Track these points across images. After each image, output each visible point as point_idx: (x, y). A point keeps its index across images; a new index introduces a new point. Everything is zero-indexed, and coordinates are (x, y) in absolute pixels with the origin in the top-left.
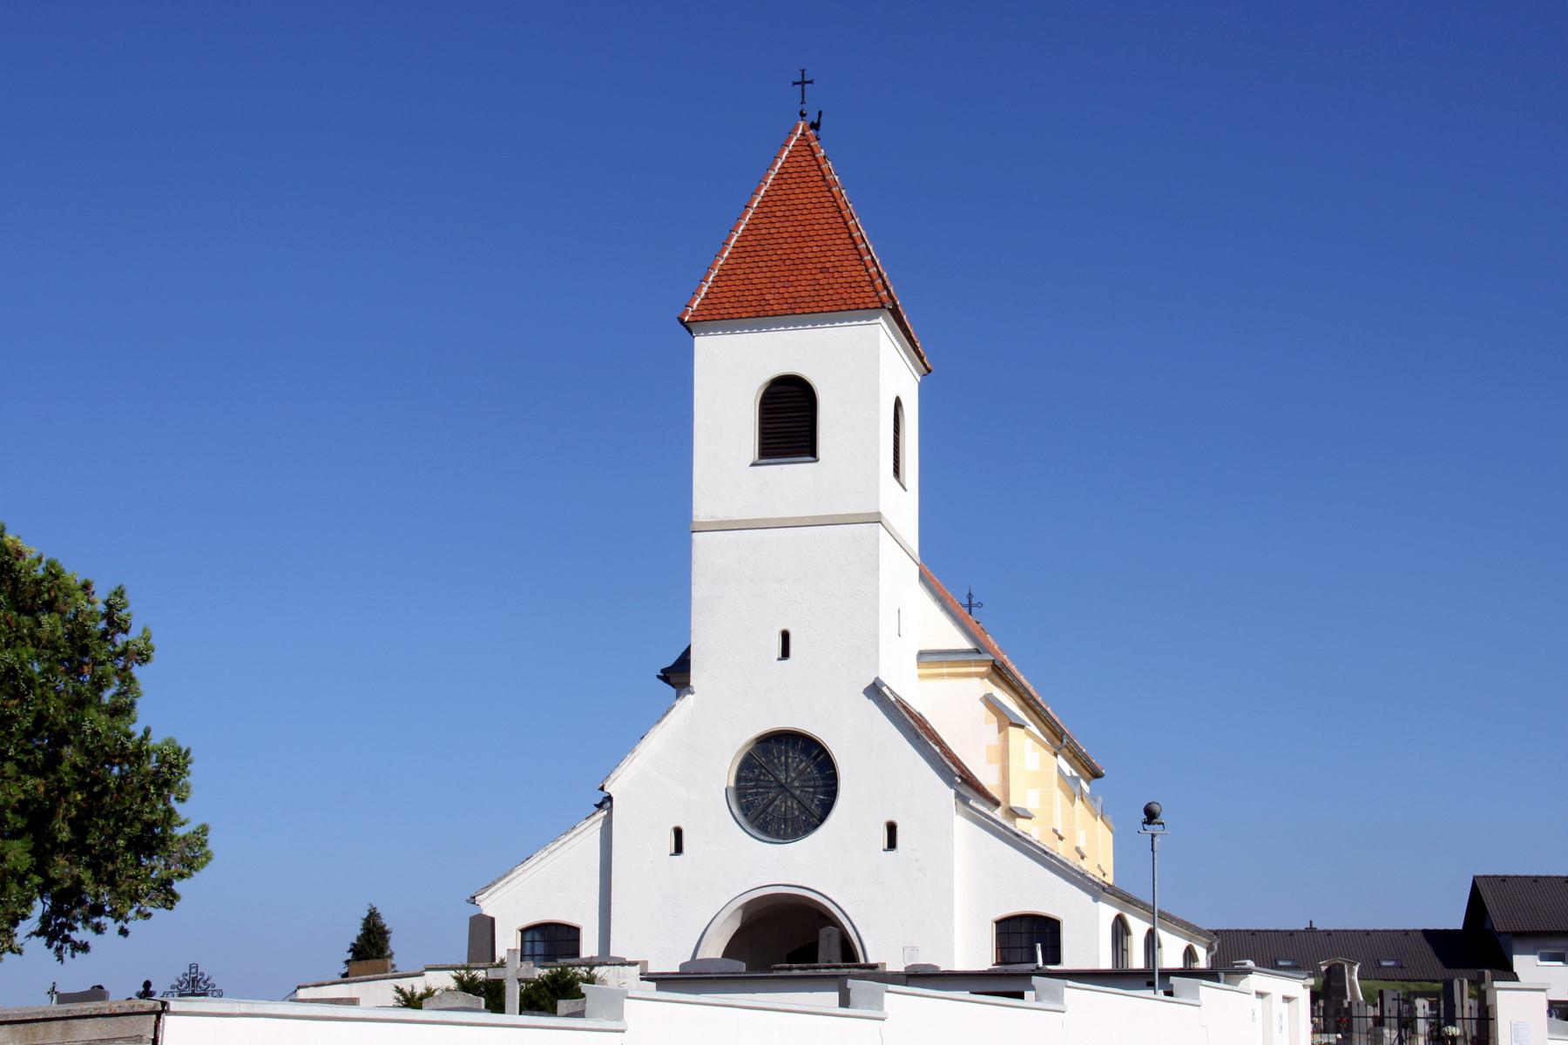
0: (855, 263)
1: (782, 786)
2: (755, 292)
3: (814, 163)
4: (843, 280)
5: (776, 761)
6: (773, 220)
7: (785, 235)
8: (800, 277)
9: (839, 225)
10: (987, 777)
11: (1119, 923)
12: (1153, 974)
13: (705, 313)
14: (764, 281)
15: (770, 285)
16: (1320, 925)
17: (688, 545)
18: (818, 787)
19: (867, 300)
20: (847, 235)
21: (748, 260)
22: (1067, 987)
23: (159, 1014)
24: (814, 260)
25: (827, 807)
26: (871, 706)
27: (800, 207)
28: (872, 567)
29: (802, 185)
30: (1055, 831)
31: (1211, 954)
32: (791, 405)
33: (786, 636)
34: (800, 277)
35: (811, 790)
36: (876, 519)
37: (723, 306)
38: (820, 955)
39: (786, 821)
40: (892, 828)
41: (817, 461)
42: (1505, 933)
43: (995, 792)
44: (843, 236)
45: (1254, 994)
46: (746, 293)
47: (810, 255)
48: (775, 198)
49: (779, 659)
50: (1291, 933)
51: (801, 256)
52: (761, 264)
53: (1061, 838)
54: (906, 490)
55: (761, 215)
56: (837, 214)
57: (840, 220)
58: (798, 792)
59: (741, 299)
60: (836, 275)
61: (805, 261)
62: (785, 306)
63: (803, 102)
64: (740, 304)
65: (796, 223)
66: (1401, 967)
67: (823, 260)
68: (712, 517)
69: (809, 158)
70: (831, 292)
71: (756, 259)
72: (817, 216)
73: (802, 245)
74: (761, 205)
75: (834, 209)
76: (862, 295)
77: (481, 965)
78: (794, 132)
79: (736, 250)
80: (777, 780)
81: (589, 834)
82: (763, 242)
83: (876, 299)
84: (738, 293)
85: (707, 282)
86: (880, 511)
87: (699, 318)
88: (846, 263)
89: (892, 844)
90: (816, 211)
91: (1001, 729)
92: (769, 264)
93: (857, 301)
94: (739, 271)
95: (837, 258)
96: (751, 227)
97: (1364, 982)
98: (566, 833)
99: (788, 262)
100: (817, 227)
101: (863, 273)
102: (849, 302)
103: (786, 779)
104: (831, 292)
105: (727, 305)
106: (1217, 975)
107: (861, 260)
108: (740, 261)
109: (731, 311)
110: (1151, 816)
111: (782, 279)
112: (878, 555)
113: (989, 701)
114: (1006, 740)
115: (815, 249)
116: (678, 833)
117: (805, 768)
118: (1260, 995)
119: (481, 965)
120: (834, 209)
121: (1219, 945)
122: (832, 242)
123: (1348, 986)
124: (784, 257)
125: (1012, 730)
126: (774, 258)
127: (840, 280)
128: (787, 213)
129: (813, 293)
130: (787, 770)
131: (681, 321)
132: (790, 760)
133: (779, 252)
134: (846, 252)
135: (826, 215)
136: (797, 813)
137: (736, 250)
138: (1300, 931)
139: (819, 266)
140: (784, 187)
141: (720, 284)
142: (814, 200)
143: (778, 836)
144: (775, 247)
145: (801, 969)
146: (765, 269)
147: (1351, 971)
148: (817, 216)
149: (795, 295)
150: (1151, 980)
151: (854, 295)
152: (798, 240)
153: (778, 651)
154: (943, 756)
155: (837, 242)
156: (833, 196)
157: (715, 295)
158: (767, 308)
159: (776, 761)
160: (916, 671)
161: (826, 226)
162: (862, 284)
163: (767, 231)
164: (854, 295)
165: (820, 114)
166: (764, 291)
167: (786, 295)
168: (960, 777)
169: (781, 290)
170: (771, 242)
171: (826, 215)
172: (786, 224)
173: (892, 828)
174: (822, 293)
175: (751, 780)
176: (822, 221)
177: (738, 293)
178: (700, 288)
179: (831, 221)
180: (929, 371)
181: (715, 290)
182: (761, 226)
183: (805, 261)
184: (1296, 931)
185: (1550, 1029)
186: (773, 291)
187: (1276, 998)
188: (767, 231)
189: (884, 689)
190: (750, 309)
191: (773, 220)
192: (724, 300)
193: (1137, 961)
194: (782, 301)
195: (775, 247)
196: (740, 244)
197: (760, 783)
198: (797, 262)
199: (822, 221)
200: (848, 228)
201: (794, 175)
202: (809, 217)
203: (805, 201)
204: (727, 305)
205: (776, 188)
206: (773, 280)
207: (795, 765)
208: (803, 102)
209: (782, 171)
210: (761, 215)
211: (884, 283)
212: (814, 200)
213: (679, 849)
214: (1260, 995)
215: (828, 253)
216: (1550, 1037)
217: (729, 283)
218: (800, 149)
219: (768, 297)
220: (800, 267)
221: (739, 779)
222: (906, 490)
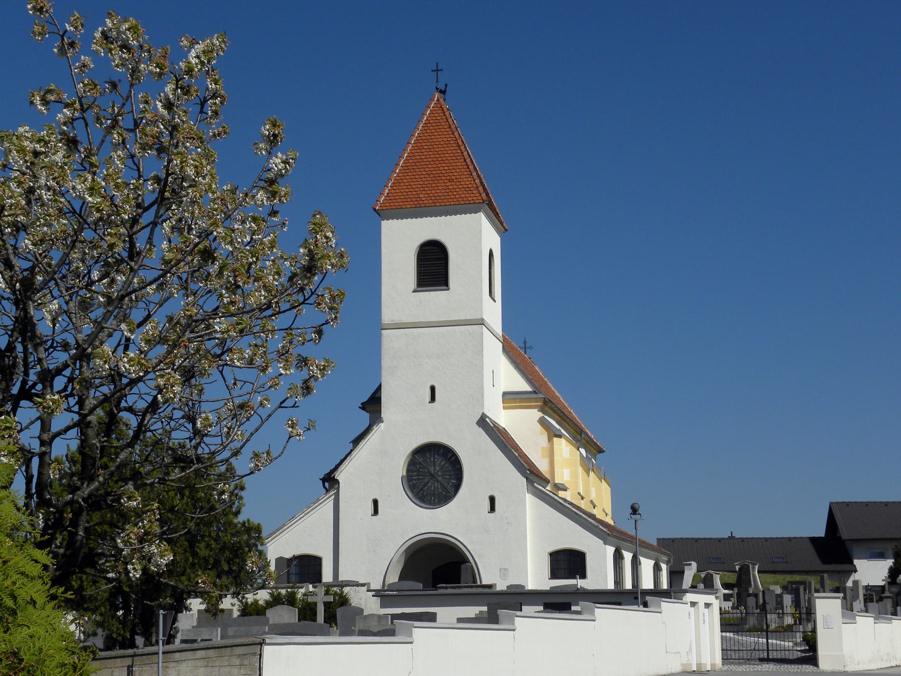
0: (468, 176)
1: (432, 475)
2: (414, 193)
3: (444, 117)
4: (462, 186)
5: (428, 460)
6: (423, 151)
7: (430, 160)
8: (438, 185)
9: (458, 154)
10: (542, 466)
11: (617, 554)
12: (638, 593)
13: (387, 205)
14: (419, 186)
15: (422, 189)
16: (737, 535)
17: (380, 337)
18: (452, 475)
19: (474, 198)
20: (463, 160)
21: (409, 174)
22: (596, 607)
23: (261, 644)
24: (446, 175)
25: (457, 487)
26: (480, 430)
27: (437, 143)
28: (479, 350)
29: (438, 130)
30: (579, 494)
31: (669, 565)
32: (433, 257)
33: (433, 389)
34: (438, 185)
35: (448, 477)
36: (481, 322)
37: (396, 201)
38: (462, 579)
39: (434, 495)
40: (492, 500)
41: (448, 289)
42: (848, 540)
43: (547, 475)
44: (461, 161)
45: (689, 604)
46: (409, 193)
47: (443, 172)
48: (423, 138)
49: (429, 402)
50: (720, 540)
51: (438, 172)
52: (417, 177)
53: (582, 498)
54: (495, 301)
55: (416, 148)
56: (457, 148)
57: (459, 151)
58: (440, 479)
59: (407, 197)
60: (458, 183)
61: (441, 175)
62: (430, 202)
63: (437, 82)
64: (406, 200)
65: (435, 153)
66: (787, 562)
67: (450, 174)
68: (392, 321)
69: (441, 114)
70: (455, 193)
71: (414, 174)
72: (447, 149)
73: (439, 165)
74: (417, 142)
75: (456, 145)
76: (472, 195)
77: (282, 585)
78: (432, 100)
79: (403, 168)
80: (429, 472)
81: (329, 505)
82: (417, 164)
83: (480, 198)
84: (404, 194)
85: (388, 187)
86: (484, 318)
87: (384, 208)
88: (462, 177)
89: (492, 509)
90: (446, 146)
91: (550, 440)
92: (421, 176)
93: (469, 199)
94: (405, 181)
95: (458, 174)
96: (411, 155)
97: (761, 575)
98: (314, 503)
99: (431, 176)
100: (446, 155)
101: (472, 182)
102: (465, 199)
103: (434, 471)
104: (455, 193)
105: (399, 200)
106: (671, 594)
107: (471, 175)
108: (406, 174)
109: (401, 204)
110: (634, 511)
111: (429, 185)
112: (482, 343)
113: (542, 422)
114: (552, 444)
115: (446, 168)
116: (375, 502)
117: (445, 465)
118: (693, 604)
119: (282, 585)
120: (456, 145)
121: (674, 559)
122: (455, 164)
123: (752, 578)
124: (429, 173)
125: (555, 440)
126: (424, 173)
127: (460, 187)
128: (430, 147)
129: (445, 194)
130: (434, 465)
131: (375, 210)
132: (436, 460)
133: (426, 170)
134: (462, 170)
135: (451, 148)
136: (440, 490)
137: (403, 168)
138: (725, 539)
139: (448, 178)
140: (428, 131)
141: (395, 188)
142: (445, 139)
143: (430, 504)
144: (424, 166)
145: (453, 588)
146: (419, 180)
147: (754, 569)
148: (447, 149)
149: (436, 195)
150: (636, 596)
151: (467, 196)
152: (437, 162)
153: (428, 398)
154: (520, 458)
155: (458, 164)
156: (455, 137)
157: (392, 195)
158: (421, 202)
159: (428, 460)
160: (502, 405)
161: (451, 155)
162: (472, 189)
163: (419, 157)
164: (467, 196)
165: (446, 85)
166: (419, 192)
167: (431, 195)
168: (529, 470)
169: (428, 192)
170: (422, 163)
171: (451, 148)
172: (430, 153)
173: (492, 500)
174: (450, 194)
175: (415, 472)
176: (449, 152)
177: (404, 194)
178: (384, 190)
179: (454, 152)
180: (506, 230)
181: (393, 191)
182: (416, 154)
183: (441, 175)
184: (723, 539)
185: (843, 616)
186: (424, 192)
187: (701, 605)
188: (419, 157)
189: (487, 419)
190: (411, 203)
191: (423, 151)
192: (397, 197)
193: (628, 585)
194: (428, 199)
195: (424, 166)
196: (405, 165)
197: (420, 473)
198: (437, 175)
199: (449, 152)
200: (463, 156)
201: (434, 125)
202: (442, 149)
203: (440, 140)
204: (399, 200)
205: (424, 132)
206: (424, 186)
207: (437, 464)
208: (437, 82)
209: (427, 122)
210: (416, 148)
211: (477, 174)
212: (445, 139)
213: (376, 512)
214: (693, 604)
215: (453, 171)
216: (844, 622)
217: (400, 188)
218: (436, 109)
219: (421, 196)
220: (438, 178)
221: (408, 471)
222: (495, 301)
